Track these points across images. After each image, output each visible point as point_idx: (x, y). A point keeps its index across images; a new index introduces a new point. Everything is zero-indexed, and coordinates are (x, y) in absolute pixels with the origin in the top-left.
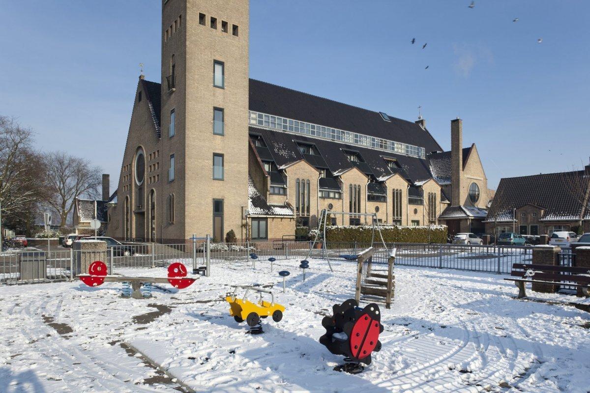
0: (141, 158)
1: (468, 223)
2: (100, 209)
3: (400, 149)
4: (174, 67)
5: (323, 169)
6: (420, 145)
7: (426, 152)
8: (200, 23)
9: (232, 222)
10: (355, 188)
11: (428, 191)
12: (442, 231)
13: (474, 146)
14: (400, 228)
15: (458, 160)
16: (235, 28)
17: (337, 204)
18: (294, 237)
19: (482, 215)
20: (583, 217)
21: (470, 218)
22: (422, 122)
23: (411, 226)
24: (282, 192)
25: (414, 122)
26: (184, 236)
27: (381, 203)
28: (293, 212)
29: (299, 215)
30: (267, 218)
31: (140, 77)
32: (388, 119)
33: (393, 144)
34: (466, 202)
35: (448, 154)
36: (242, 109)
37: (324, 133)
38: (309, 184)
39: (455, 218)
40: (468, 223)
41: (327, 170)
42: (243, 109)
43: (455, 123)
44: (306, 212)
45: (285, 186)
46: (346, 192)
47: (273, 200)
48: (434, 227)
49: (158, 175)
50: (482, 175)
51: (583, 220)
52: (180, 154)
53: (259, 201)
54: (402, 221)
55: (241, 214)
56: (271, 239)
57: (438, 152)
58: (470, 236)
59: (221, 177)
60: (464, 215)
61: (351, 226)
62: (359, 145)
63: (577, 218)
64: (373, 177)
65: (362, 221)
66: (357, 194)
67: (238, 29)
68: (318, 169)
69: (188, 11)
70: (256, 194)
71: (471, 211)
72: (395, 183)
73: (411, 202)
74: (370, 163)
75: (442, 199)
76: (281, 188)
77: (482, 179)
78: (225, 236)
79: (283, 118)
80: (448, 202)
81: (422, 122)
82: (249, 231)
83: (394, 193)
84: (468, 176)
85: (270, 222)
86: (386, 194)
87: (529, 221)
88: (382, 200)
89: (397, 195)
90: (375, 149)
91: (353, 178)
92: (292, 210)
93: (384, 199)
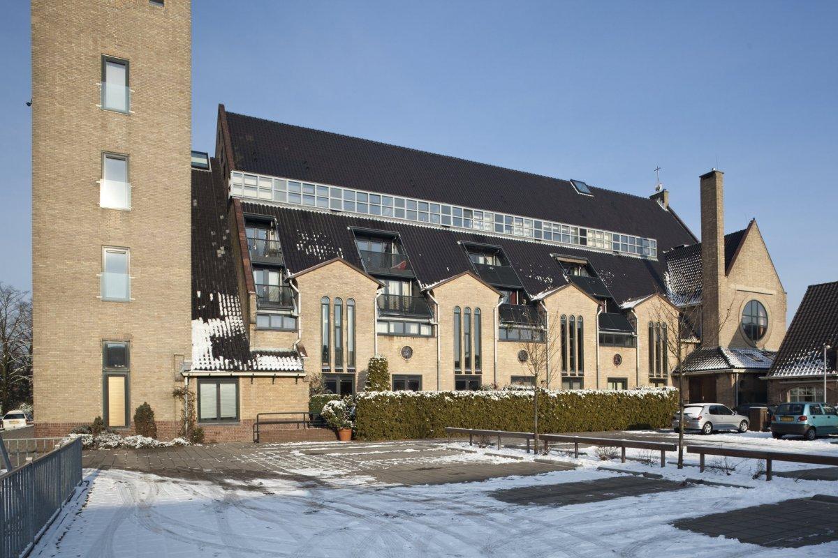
1: (733, 382)
5: (407, 280)
9: (152, 386)
12: (664, 400)
13: (754, 226)
15: (715, 255)
19: (767, 363)
21: (735, 371)
22: (661, 196)
23: (609, 389)
25: (648, 198)
27: (624, 349)
30: (238, 377)
33: (583, 233)
36: (174, 155)
37: (391, 209)
38: (479, 316)
39: (703, 372)
40: (733, 382)
41: (609, 300)
42: (178, 156)
43: (709, 179)
45: (432, 321)
50: (775, 284)
56: (245, 421)
57: (685, 246)
58: (713, 411)
60: (723, 365)
62: (505, 235)
65: (486, 379)
70: (239, 331)
72: (567, 303)
73: (604, 341)
77: (775, 292)
81: (661, 196)
83: (563, 327)
84: (736, 290)
85: (246, 386)
89: (572, 331)
93: (631, 342)
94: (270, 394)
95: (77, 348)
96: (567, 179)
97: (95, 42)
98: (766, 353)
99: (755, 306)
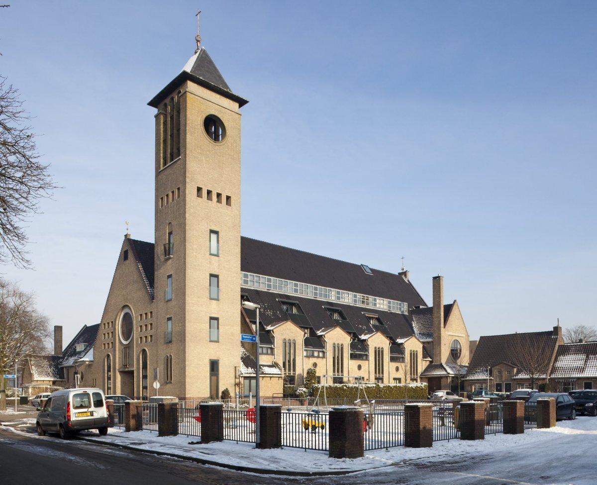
0: (127, 319)
1: (449, 381)
2: (54, 365)
3: (382, 304)
4: (170, 234)
6: (403, 301)
7: (409, 307)
8: (198, 196)
9: (227, 381)
10: (338, 347)
11: (410, 349)
12: (422, 389)
13: (456, 303)
14: (381, 385)
16: (228, 198)
17: (321, 362)
18: (282, 395)
19: (463, 372)
20: (550, 376)
21: (450, 375)
22: (405, 273)
23: (393, 384)
24: (269, 351)
26: (185, 395)
28: (281, 371)
29: (286, 374)
31: (126, 236)
32: (370, 271)
33: (375, 300)
34: (447, 359)
35: (430, 310)
37: (307, 291)
38: (295, 344)
39: (437, 376)
40: (449, 381)
41: (311, 329)
43: (437, 280)
44: (287, 371)
45: (273, 346)
46: (299, 345)
47: (264, 360)
48: (413, 385)
49: (151, 336)
51: (549, 378)
52: (180, 316)
53: (250, 361)
54: (384, 379)
55: (234, 374)
57: (421, 307)
58: (448, 394)
59: (216, 339)
61: (336, 384)
63: (544, 376)
64: (355, 336)
65: (345, 379)
66: (340, 352)
67: (231, 200)
68: (302, 328)
69: (187, 185)
70: (245, 354)
71: (452, 368)
72: (377, 341)
73: (393, 359)
74: (354, 322)
75: (424, 357)
76: (269, 348)
78: (220, 394)
79: (267, 277)
80: (430, 359)
81: (405, 273)
82: (242, 390)
86: (368, 353)
87: (504, 379)
88: (364, 358)
89: (379, 353)
90: (357, 306)
91: (336, 337)
92: (280, 369)
93: (366, 357)
94: (269, 385)
95: (201, 363)
96: (360, 264)
97: (207, 223)
98: (461, 366)
99: (456, 342)
